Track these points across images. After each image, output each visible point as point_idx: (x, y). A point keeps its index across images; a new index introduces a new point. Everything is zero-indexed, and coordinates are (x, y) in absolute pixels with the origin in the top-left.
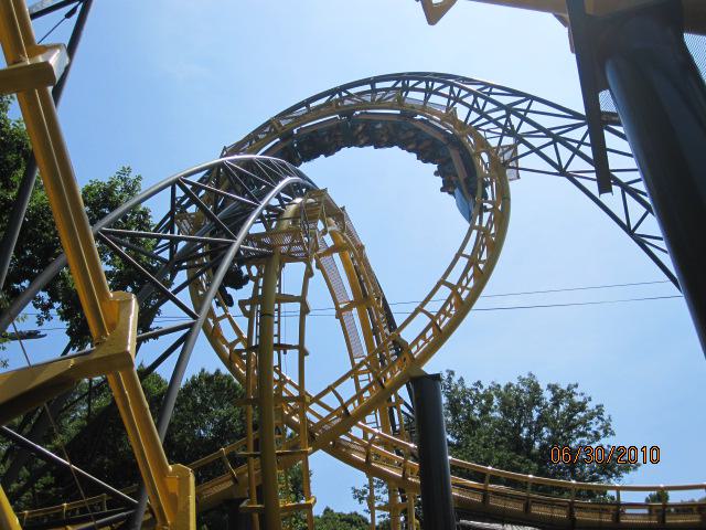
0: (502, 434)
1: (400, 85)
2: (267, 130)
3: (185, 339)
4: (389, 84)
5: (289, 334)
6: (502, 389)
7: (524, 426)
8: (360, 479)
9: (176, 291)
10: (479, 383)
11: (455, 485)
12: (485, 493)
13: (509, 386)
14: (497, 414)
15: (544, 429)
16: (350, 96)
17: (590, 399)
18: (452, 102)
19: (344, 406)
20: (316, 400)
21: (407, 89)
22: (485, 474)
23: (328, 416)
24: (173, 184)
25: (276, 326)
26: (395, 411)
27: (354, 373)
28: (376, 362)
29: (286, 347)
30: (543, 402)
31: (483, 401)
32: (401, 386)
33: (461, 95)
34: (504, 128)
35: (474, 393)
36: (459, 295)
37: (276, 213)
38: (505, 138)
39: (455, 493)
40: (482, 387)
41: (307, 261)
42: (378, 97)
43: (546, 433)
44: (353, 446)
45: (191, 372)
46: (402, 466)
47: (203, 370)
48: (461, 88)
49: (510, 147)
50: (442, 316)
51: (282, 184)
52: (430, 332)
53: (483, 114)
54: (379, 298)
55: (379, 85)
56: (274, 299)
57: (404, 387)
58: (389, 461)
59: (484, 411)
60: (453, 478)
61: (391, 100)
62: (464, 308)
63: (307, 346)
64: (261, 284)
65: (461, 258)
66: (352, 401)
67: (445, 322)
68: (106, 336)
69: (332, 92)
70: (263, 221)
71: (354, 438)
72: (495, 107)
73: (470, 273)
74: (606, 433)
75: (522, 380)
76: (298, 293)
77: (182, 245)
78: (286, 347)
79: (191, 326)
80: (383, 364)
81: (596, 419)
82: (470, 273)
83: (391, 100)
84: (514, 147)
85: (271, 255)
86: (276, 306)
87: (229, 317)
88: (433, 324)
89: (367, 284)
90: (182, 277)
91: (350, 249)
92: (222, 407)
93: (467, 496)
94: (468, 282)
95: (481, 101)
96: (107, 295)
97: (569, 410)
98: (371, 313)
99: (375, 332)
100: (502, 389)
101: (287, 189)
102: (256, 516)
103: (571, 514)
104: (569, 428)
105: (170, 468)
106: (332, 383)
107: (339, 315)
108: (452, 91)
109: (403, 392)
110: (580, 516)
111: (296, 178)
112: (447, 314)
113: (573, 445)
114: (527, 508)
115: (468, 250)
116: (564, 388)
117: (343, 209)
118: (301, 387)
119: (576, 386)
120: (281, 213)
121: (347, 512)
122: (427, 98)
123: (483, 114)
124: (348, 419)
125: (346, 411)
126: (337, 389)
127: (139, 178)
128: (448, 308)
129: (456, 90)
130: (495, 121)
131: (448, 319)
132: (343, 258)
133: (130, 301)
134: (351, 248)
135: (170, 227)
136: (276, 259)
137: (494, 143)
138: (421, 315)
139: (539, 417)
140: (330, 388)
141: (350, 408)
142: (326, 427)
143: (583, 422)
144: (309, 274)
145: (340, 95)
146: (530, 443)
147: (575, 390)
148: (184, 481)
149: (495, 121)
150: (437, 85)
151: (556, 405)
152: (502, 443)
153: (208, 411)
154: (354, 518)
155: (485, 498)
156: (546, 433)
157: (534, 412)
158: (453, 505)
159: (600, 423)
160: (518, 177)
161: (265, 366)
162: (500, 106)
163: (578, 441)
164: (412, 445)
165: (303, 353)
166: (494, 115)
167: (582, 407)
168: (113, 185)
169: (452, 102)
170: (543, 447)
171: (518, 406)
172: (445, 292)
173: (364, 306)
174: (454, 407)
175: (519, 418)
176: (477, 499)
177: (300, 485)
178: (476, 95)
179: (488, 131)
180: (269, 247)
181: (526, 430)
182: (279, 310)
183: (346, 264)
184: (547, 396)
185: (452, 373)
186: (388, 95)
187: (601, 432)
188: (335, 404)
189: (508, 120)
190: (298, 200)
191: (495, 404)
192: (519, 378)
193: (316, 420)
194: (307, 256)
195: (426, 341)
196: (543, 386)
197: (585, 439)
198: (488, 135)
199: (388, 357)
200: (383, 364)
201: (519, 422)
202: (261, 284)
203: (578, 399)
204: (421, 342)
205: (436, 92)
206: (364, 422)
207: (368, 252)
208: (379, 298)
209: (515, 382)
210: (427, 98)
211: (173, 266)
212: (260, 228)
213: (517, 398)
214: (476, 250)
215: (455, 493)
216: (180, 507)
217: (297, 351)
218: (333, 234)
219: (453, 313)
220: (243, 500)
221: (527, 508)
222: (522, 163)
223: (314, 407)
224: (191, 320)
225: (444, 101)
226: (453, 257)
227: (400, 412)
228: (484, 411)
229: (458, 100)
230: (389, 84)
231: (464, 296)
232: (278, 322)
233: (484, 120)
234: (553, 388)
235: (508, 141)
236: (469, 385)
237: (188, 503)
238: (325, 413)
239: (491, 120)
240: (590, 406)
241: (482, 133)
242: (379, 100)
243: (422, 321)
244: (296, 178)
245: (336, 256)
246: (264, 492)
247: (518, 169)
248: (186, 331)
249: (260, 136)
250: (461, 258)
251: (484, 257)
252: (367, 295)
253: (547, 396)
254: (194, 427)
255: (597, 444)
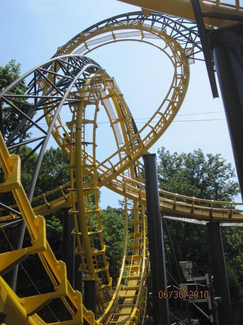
0: (185, 177)
1: (140, 17)
2: (78, 38)
3: (42, 143)
4: (136, 16)
5: (88, 137)
6: (186, 156)
7: (196, 172)
8: (122, 198)
9: (37, 121)
10: (176, 153)
11: (162, 201)
12: (174, 205)
13: (189, 155)
14: (184, 167)
15: (204, 174)
16: (117, 22)
17: (225, 161)
18: (164, 26)
19: (113, 168)
20: (102, 164)
21: (143, 19)
22: (174, 197)
23: (107, 171)
24: (34, 71)
25: (83, 134)
26: (137, 167)
27: (118, 152)
28: (129, 147)
29: (87, 143)
30: (205, 162)
31: (178, 161)
32: (140, 157)
33: (169, 23)
34: (188, 39)
35: (174, 157)
36: (165, 118)
37: (82, 83)
38: (188, 44)
39: (161, 204)
40: (177, 155)
41: (96, 104)
42: (130, 23)
43: (206, 175)
44: (117, 184)
45: (48, 148)
46: (139, 193)
47: (52, 148)
48: (169, 19)
49: (191, 49)
50: (157, 127)
51: (85, 67)
52: (152, 135)
53: (179, 32)
54: (130, 118)
55: (130, 17)
56: (81, 122)
57: (141, 158)
58: (134, 191)
59: (178, 166)
60: (160, 198)
61: (136, 24)
62: (167, 124)
63: (97, 143)
64: (76, 115)
65: (166, 101)
66: (117, 165)
67: (158, 130)
68: (9, 175)
69: (108, 20)
70: (76, 86)
71: (118, 181)
72: (184, 29)
73: (171, 107)
74: (232, 175)
75: (195, 152)
76: (92, 119)
77: (40, 94)
78: (87, 143)
79: (45, 137)
80: (132, 147)
81: (227, 169)
82: (171, 107)
83: (136, 24)
84: (192, 49)
85: (80, 102)
86: (83, 125)
87: (62, 127)
88: (153, 131)
89: (124, 111)
90: (40, 113)
91: (114, 96)
92: (61, 164)
93: (166, 206)
94: (169, 112)
95: (178, 26)
96: (8, 156)
97: (216, 165)
98: (126, 125)
99: (128, 132)
100: (186, 156)
101: (87, 70)
102: (75, 216)
103: (211, 214)
104: (216, 173)
105: (36, 217)
106: (108, 157)
107: (112, 126)
108: (164, 20)
109: (141, 160)
110: (214, 215)
111: (92, 65)
112: (160, 126)
113: (217, 181)
114: (192, 211)
115: (170, 98)
116: (214, 155)
117: (113, 78)
118: (94, 158)
119: (220, 155)
120: (85, 82)
121: (117, 208)
122: (153, 24)
123: (179, 32)
124: (115, 173)
125: (114, 169)
126: (110, 160)
127: (19, 64)
128: (160, 124)
129: (166, 20)
130: (184, 36)
131: (160, 128)
132: (113, 100)
133: (17, 159)
134: (117, 96)
135: (34, 85)
136: (82, 104)
137: (183, 46)
138: (148, 127)
139: (202, 169)
140: (107, 160)
141: (116, 168)
142: (107, 176)
143: (223, 171)
144: (97, 110)
145: (112, 22)
146: (198, 180)
147: (219, 157)
148: (41, 222)
149: (184, 36)
150: (157, 18)
151: (210, 163)
152: (184, 180)
153: (54, 165)
154: (121, 211)
155: (174, 207)
156: (206, 175)
157: (200, 166)
158: (160, 210)
159: (230, 171)
160: (194, 63)
161: (78, 152)
162: (186, 29)
163: (219, 179)
164: (143, 184)
165: (95, 146)
166: (184, 33)
167: (222, 165)
168: (7, 68)
169: (164, 26)
170: (204, 182)
171: (193, 164)
172: (159, 117)
173: (123, 121)
174: (164, 163)
175: (194, 168)
176: (171, 207)
177: (95, 199)
178: (176, 23)
179: (182, 40)
180: (79, 98)
181: (196, 174)
182: (84, 126)
183: (115, 103)
184: (207, 159)
185: (164, 148)
186: (135, 22)
187: (230, 175)
188: (110, 167)
189: (190, 35)
190: (92, 75)
191: (183, 162)
192: (194, 151)
193: (101, 173)
194: (96, 102)
195: (150, 138)
196: (205, 155)
197: (223, 178)
198: (181, 42)
199: (134, 144)
200: (132, 147)
201: (194, 170)
202: (76, 115)
203: (220, 160)
204: (148, 139)
205: (157, 21)
206: (123, 174)
207: (126, 98)
208: (130, 118)
209: (192, 153)
210: (153, 24)
211: (36, 107)
212: (75, 89)
213: (193, 160)
214: (173, 97)
215: (161, 204)
216: (40, 232)
217: (92, 145)
218: (109, 90)
219: (162, 125)
220: (69, 208)
221: (192, 211)
222: (196, 56)
223: (101, 167)
224: (44, 135)
225: (160, 25)
226: (154, 113)
227: (139, 168)
228: (178, 166)
229: (167, 25)
230: (136, 16)
231: (167, 119)
232: (84, 132)
233: (179, 35)
234: (209, 156)
235: (190, 45)
236: (171, 154)
237: (43, 231)
238: (105, 170)
239: (182, 35)
240: (226, 164)
241: (177, 41)
242: (131, 24)
243: (148, 130)
244: (92, 65)
245: (110, 99)
246: (78, 205)
247: (193, 58)
248: (43, 139)
249: (76, 42)
250: (166, 101)
251: (177, 100)
252: (124, 117)
253: (207, 159)
254: (48, 173)
255: (228, 180)
